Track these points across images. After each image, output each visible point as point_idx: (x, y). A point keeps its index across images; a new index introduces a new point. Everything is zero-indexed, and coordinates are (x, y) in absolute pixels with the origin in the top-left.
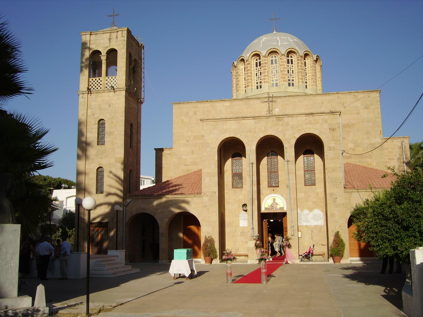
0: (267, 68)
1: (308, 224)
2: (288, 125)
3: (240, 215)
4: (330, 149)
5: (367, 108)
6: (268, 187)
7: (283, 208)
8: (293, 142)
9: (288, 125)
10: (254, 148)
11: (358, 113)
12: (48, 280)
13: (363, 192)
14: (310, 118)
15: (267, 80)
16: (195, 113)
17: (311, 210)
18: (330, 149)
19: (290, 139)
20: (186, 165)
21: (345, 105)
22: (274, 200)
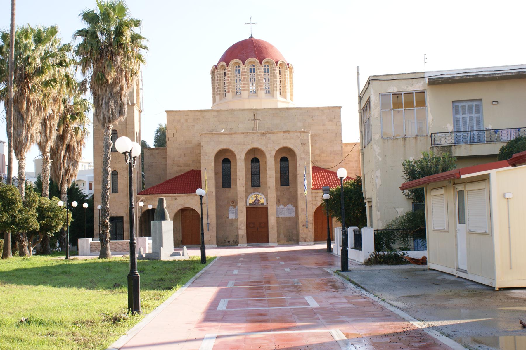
0: (246, 76)
1: (283, 216)
2: (270, 139)
3: (229, 209)
4: (301, 159)
5: (331, 121)
6: (252, 187)
7: (263, 204)
8: (274, 153)
9: (270, 139)
10: (243, 157)
11: (324, 125)
12: (350, 271)
13: (291, 83)
14: (287, 135)
15: (246, 88)
16: (186, 120)
17: (285, 205)
18: (301, 159)
19: (271, 151)
20: (178, 166)
21: (314, 118)
22: (257, 197)
